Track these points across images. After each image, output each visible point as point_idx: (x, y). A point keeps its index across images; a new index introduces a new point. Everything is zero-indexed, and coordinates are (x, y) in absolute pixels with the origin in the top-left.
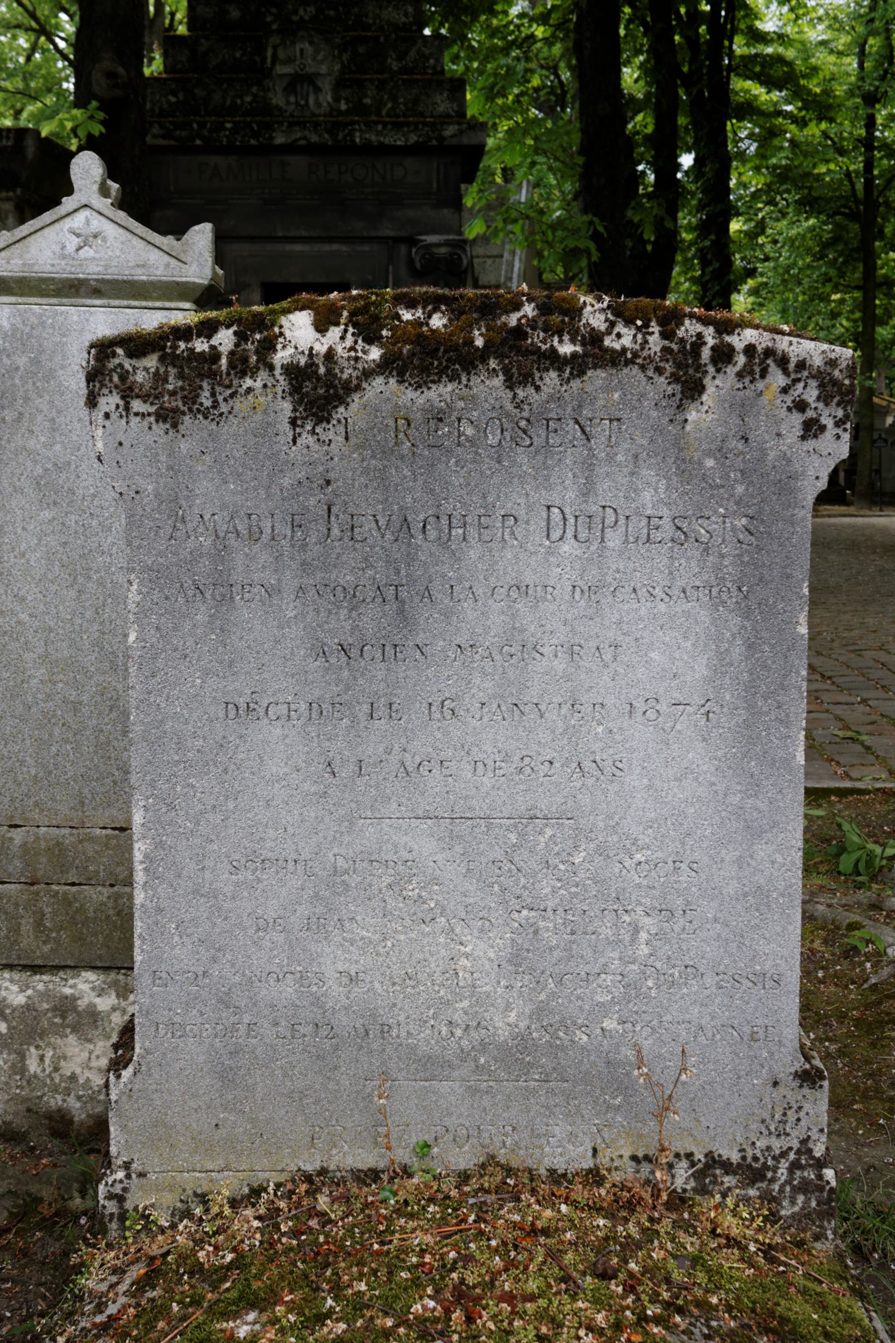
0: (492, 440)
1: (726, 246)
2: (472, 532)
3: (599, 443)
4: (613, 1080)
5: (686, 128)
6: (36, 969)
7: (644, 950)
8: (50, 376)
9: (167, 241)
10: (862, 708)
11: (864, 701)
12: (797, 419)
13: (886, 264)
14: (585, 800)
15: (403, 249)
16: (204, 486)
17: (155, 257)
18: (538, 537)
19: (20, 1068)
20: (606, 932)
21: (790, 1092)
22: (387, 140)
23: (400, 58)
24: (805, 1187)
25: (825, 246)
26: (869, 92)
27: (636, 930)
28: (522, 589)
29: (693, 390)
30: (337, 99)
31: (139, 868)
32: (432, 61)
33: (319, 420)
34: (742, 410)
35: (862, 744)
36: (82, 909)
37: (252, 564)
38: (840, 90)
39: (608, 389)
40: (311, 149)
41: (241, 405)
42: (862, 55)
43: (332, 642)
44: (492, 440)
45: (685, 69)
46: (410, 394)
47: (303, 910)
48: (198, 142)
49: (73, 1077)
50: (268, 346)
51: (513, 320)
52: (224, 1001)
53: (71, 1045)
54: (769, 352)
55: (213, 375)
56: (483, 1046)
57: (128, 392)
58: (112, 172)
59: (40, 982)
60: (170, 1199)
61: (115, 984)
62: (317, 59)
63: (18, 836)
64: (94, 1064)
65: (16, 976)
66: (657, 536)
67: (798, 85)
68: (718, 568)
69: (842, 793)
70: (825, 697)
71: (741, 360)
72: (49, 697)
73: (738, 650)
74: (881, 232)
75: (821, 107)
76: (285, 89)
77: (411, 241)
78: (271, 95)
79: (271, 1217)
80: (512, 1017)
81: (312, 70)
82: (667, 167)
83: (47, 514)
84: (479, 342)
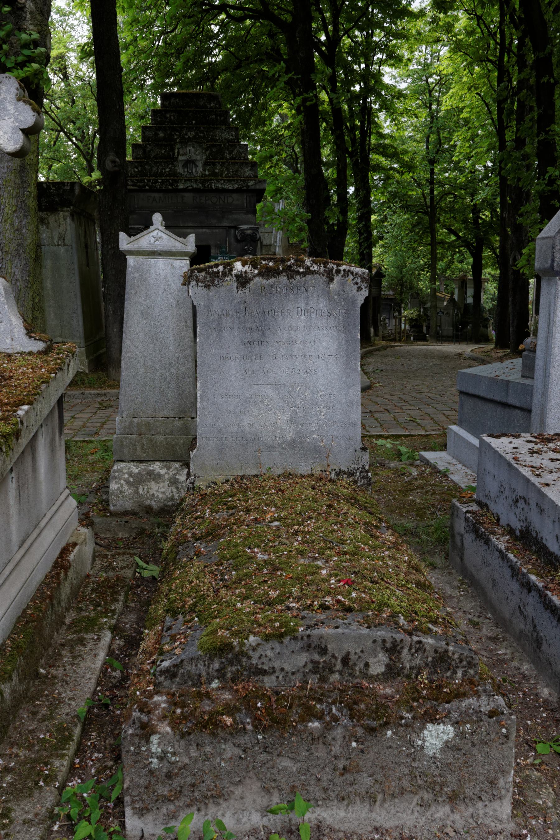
0: (284, 292)
1: (369, 227)
2: (280, 314)
3: (309, 293)
4: (315, 451)
5: (351, 175)
6: (141, 461)
7: (323, 417)
8: (145, 280)
9: (181, 239)
10: (418, 411)
11: (419, 409)
12: (356, 286)
13: (442, 234)
14: (308, 379)
15: (232, 231)
16: (216, 303)
17: (177, 244)
18: (295, 315)
19: (137, 492)
20: (314, 412)
21: (359, 453)
22: (226, 187)
23: (230, 153)
24: (363, 478)
25: (414, 226)
26: (431, 159)
27: (321, 412)
28: (292, 328)
29: (331, 280)
30: (204, 170)
31: (198, 398)
32: (243, 155)
33: (243, 287)
34: (343, 284)
35: (417, 423)
36: (156, 443)
37: (227, 322)
38: (418, 158)
39: (311, 280)
40: (194, 190)
41: (224, 284)
42: (427, 142)
43: (246, 341)
44: (284, 292)
45: (350, 150)
46: (265, 281)
47: (239, 408)
48: (147, 188)
49: (153, 495)
50: (231, 270)
51: (289, 263)
52: (220, 432)
53: (153, 484)
54: (349, 271)
55: (218, 277)
56: (284, 442)
57: (198, 281)
58: (164, 219)
59: (143, 466)
60: (205, 483)
61: (166, 466)
62: (195, 153)
63: (136, 420)
64: (160, 490)
65: (135, 464)
66: (324, 314)
67: (399, 158)
68: (338, 322)
69: (406, 436)
70: (404, 408)
71: (342, 273)
72: (145, 377)
73: (344, 342)
74: (439, 220)
75: (409, 167)
76: (183, 166)
77: (236, 228)
78: (177, 168)
79: (232, 484)
80: (291, 434)
81: (194, 158)
82: (342, 194)
83: (144, 322)
84: (281, 269)
